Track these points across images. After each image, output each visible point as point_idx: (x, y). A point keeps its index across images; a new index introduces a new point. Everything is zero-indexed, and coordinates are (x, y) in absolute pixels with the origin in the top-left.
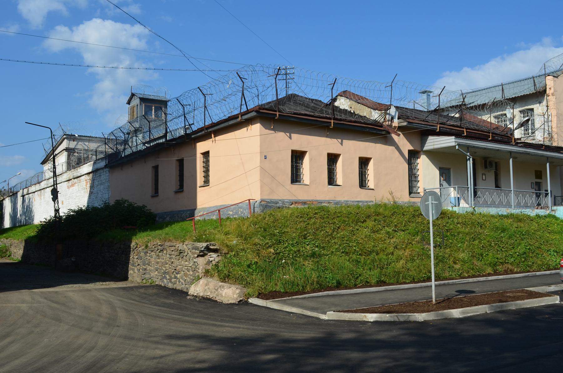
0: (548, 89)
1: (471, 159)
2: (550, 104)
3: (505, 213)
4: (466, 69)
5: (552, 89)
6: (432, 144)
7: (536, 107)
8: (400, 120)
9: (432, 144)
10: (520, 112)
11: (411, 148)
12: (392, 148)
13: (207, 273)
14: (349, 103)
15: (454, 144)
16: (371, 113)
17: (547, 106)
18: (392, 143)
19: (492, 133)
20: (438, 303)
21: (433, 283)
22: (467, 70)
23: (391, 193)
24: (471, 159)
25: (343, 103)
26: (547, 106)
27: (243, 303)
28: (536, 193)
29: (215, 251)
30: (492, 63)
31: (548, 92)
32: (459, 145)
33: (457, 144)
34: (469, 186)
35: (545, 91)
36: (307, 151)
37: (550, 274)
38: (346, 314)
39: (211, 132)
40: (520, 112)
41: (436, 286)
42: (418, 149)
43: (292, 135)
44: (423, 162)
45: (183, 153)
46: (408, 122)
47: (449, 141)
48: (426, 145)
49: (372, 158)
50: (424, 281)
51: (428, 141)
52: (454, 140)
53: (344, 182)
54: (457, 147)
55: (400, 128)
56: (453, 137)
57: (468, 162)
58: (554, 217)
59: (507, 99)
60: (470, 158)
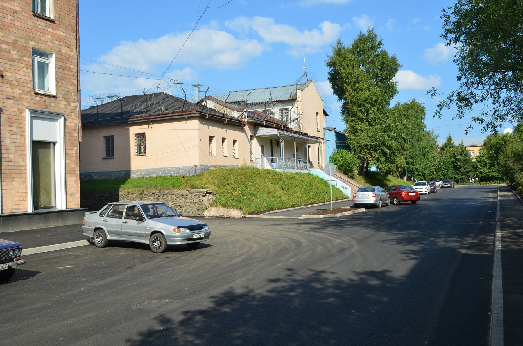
0: (298, 98)
1: (283, 142)
2: (299, 107)
3: (294, 172)
4: (141, 40)
5: (301, 98)
6: (262, 132)
7: (290, 107)
8: (248, 118)
9: (262, 132)
10: (280, 109)
11: (251, 134)
12: (244, 134)
13: (211, 205)
14: (214, 105)
15: (276, 133)
16: (231, 113)
17: (297, 108)
18: (243, 130)
19: (283, 126)
20: (333, 211)
21: (332, 202)
22: (142, 42)
23: (244, 161)
24: (283, 142)
25: (210, 104)
26: (297, 108)
27: (244, 217)
28: (299, 160)
29: (210, 193)
30: (165, 38)
31: (298, 99)
32: (279, 134)
33: (278, 133)
34: (282, 157)
35: (296, 99)
36: (236, 139)
37: (323, 205)
38: (311, 216)
39: (150, 121)
40: (280, 109)
41: (333, 203)
42: (253, 135)
43: (228, 130)
44: (255, 141)
45: (115, 132)
46: (254, 120)
47: (273, 132)
48: (258, 132)
49: (237, 140)
50: (329, 201)
51: (259, 131)
52: (277, 131)
53: (217, 154)
54: (278, 135)
55: (248, 123)
56: (276, 129)
57: (281, 143)
58: (311, 174)
59: (273, 101)
60: (282, 141)
